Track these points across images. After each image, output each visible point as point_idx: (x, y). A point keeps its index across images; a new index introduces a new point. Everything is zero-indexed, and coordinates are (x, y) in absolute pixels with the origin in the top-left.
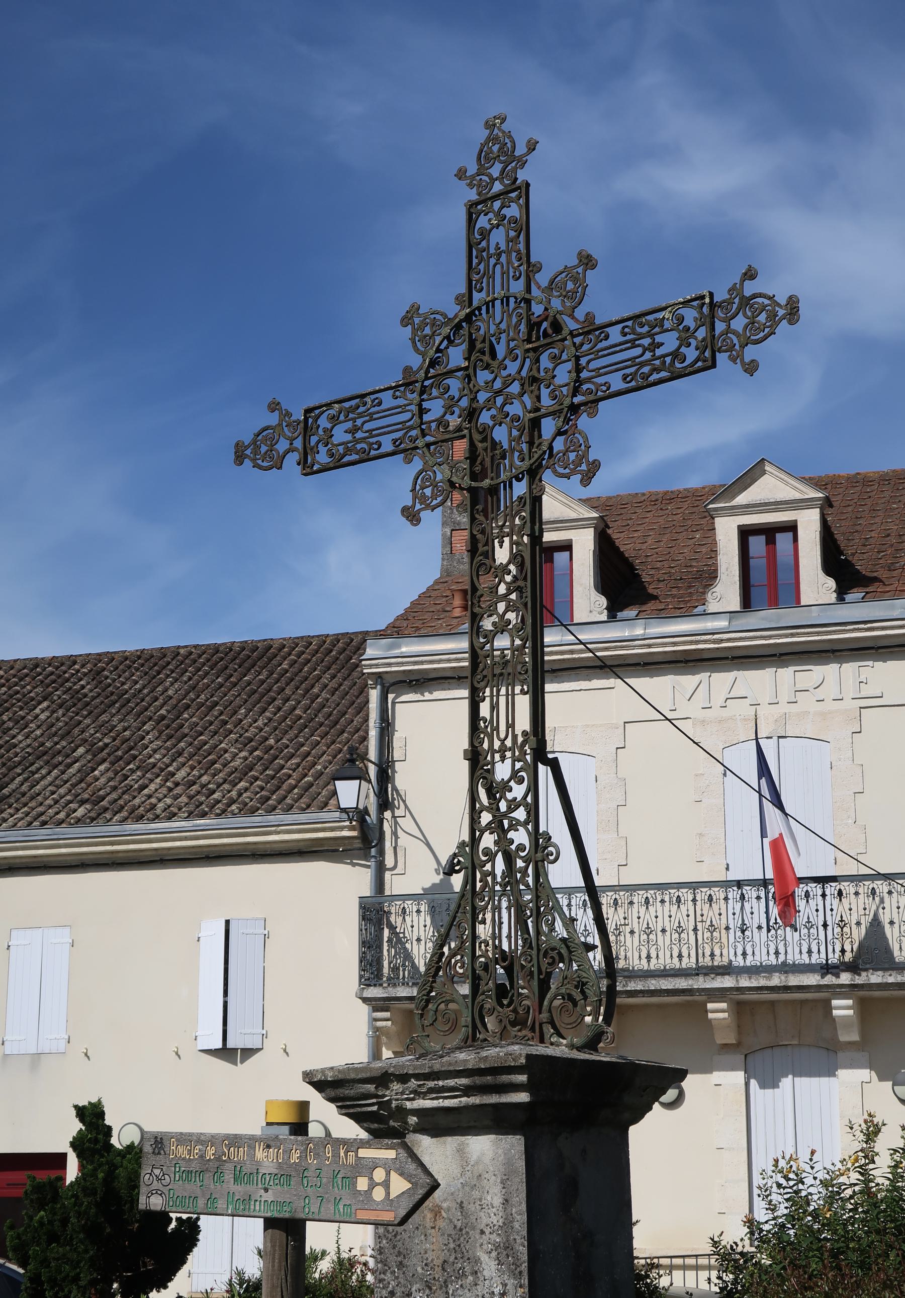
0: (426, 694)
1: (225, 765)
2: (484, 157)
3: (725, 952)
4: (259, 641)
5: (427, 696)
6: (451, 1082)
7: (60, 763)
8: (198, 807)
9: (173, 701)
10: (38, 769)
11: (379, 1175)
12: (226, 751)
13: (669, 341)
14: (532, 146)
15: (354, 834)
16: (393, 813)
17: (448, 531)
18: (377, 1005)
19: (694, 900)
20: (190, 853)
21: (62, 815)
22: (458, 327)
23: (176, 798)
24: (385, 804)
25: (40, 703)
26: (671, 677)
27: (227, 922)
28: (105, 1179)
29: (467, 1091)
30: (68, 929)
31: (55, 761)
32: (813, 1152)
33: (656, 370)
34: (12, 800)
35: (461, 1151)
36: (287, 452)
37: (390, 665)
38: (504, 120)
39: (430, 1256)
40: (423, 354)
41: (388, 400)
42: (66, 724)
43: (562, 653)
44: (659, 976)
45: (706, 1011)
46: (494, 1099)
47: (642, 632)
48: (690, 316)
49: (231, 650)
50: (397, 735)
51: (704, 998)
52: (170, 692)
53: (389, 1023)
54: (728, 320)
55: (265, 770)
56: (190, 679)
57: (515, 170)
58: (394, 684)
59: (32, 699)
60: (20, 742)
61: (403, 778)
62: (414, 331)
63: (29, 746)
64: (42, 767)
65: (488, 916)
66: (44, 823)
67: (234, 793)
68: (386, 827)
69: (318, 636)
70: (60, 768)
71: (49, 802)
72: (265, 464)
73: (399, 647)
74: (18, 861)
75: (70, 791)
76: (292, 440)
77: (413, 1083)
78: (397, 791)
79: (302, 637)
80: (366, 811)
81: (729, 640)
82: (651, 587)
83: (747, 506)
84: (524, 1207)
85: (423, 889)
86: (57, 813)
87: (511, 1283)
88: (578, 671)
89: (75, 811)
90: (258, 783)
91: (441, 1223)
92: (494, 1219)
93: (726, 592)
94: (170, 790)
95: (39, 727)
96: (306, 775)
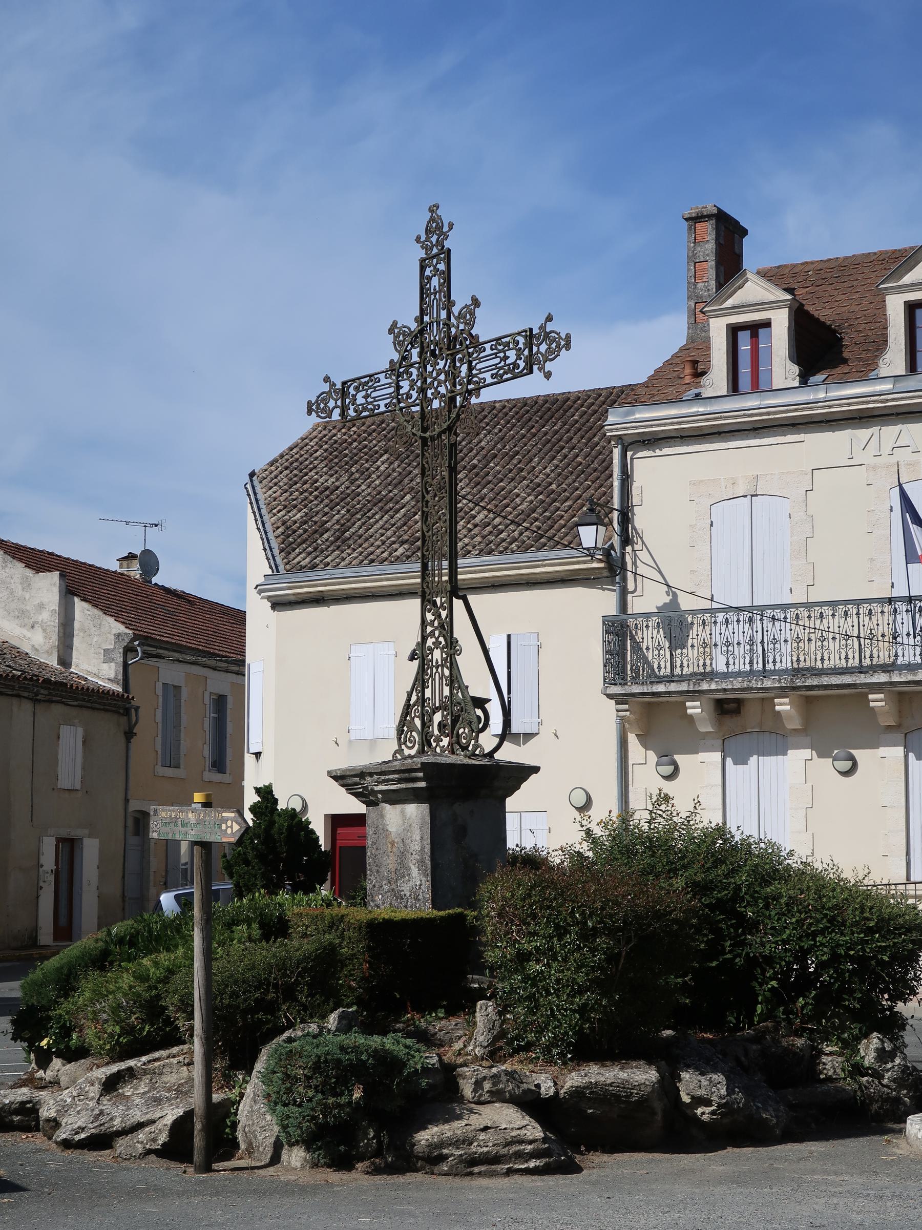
0: (657, 451)
1: (514, 509)
2: (428, 231)
3: (881, 654)
4: (559, 394)
5: (658, 452)
6: (391, 777)
7: (391, 509)
8: (487, 545)
9: (484, 452)
10: (374, 515)
11: (229, 823)
12: (518, 495)
13: (512, 354)
14: (451, 226)
15: (602, 565)
16: (633, 547)
17: (692, 304)
18: (620, 699)
19: (858, 614)
20: (480, 583)
21: (386, 555)
22: (416, 336)
23: (473, 538)
24: (626, 540)
25: (381, 456)
26: (848, 432)
27: (509, 636)
28: (265, 829)
29: (400, 781)
30: (392, 643)
31: (387, 507)
32: (610, 812)
33: (506, 373)
34: (351, 542)
35: (403, 812)
36: (334, 408)
37: (626, 429)
38: (438, 208)
39: (390, 866)
40: (399, 352)
42: (400, 473)
43: (761, 414)
44: (829, 674)
45: (868, 701)
46: (411, 785)
47: (824, 396)
48: (521, 340)
49: (536, 403)
50: (635, 485)
51: (867, 690)
52: (483, 444)
53: (628, 713)
54: (538, 346)
55: (544, 512)
56: (500, 430)
58: (631, 444)
59: (377, 452)
60: (363, 491)
61: (640, 520)
62: (395, 337)
63: (369, 494)
64: (377, 513)
65: (430, 684)
66: (372, 561)
67: (516, 533)
68: (628, 559)
69: (606, 389)
70: (391, 513)
71: (378, 543)
72: (323, 415)
73: (634, 414)
74: (353, 592)
75: (395, 533)
76: (336, 401)
77: (375, 777)
78: (636, 530)
79: (594, 390)
80: (612, 547)
81: (893, 400)
82: (847, 350)
83: (912, 285)
84: (429, 841)
85: (657, 608)
86: (383, 552)
87: (424, 879)
88: (775, 429)
89: (396, 550)
90: (537, 523)
91: (395, 850)
92: (417, 847)
93: (894, 360)
94: (470, 530)
95: (378, 477)
96: (574, 516)
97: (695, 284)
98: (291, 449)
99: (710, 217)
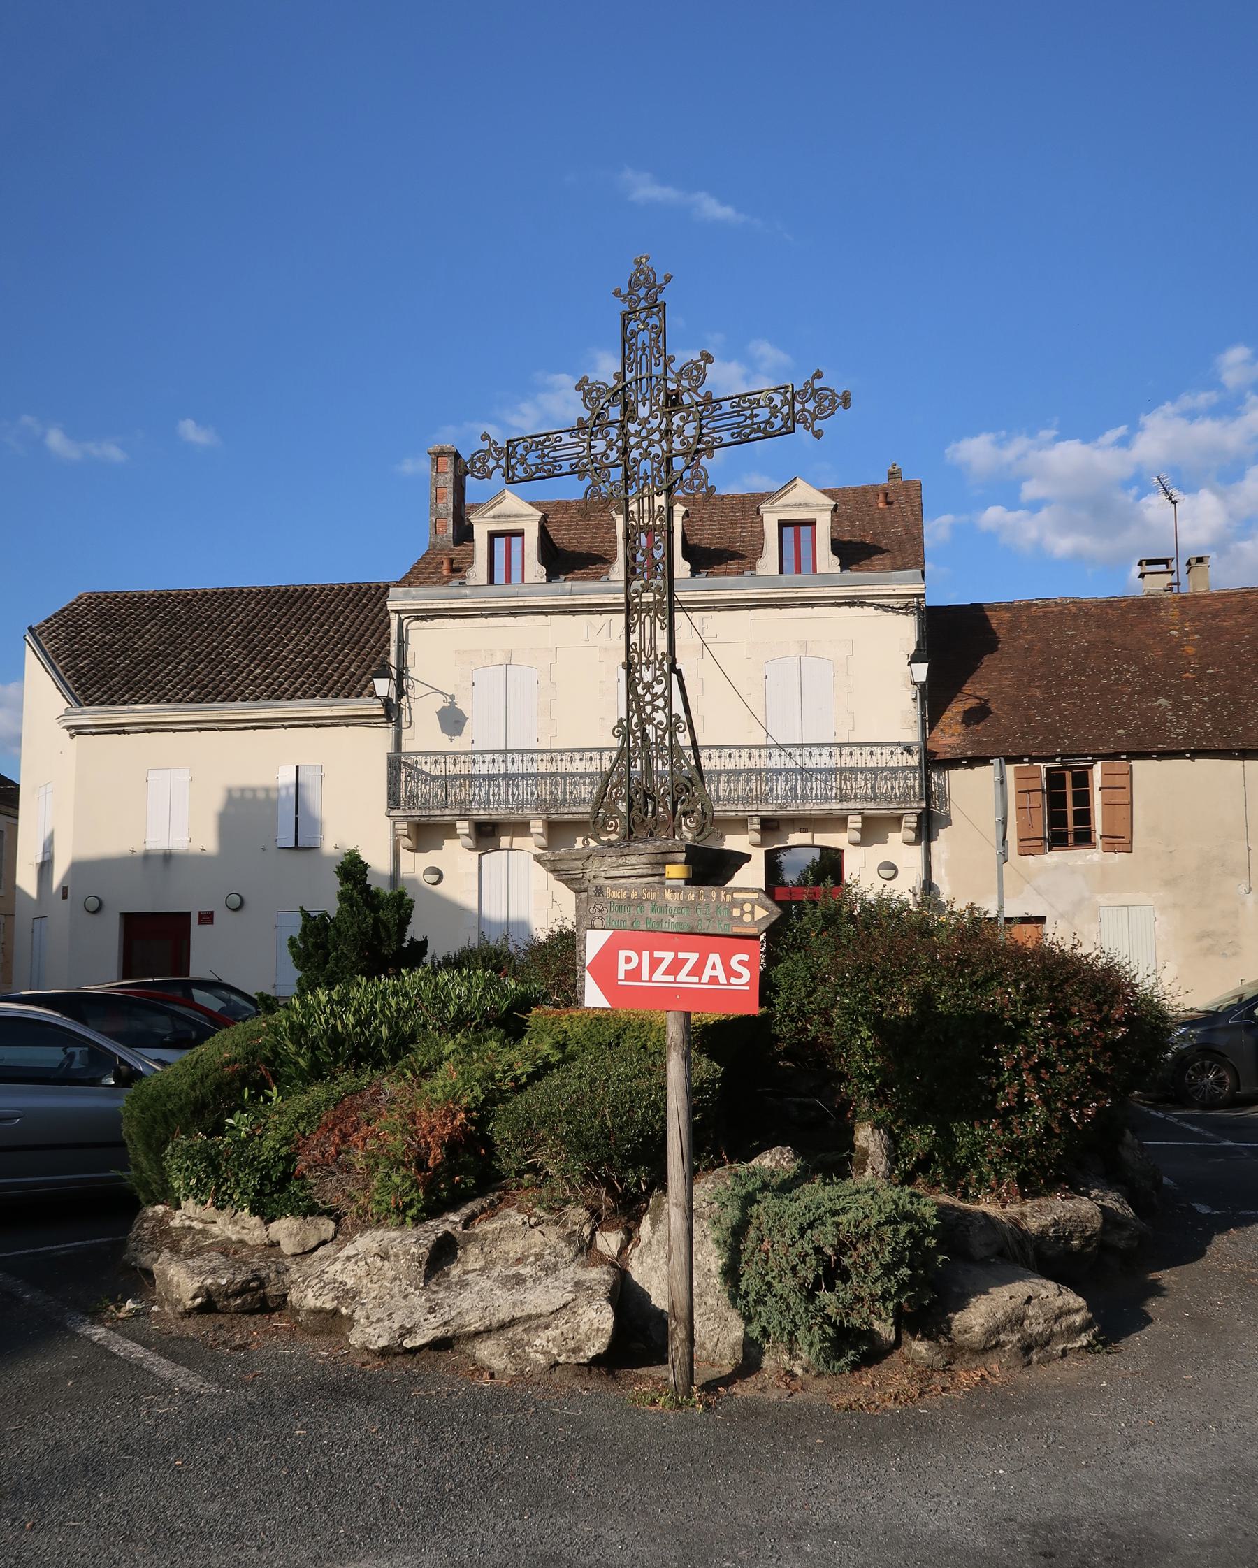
11: (747, 907)
33: (753, 431)
36: (494, 468)
41: (566, 438)
54: (803, 403)
57: (656, 293)
76: (498, 460)
97: (436, 504)
98: (62, 611)
99: (449, 453)
